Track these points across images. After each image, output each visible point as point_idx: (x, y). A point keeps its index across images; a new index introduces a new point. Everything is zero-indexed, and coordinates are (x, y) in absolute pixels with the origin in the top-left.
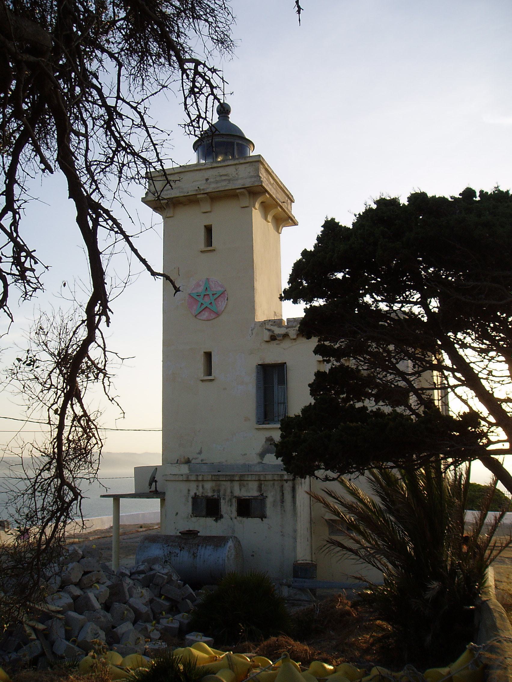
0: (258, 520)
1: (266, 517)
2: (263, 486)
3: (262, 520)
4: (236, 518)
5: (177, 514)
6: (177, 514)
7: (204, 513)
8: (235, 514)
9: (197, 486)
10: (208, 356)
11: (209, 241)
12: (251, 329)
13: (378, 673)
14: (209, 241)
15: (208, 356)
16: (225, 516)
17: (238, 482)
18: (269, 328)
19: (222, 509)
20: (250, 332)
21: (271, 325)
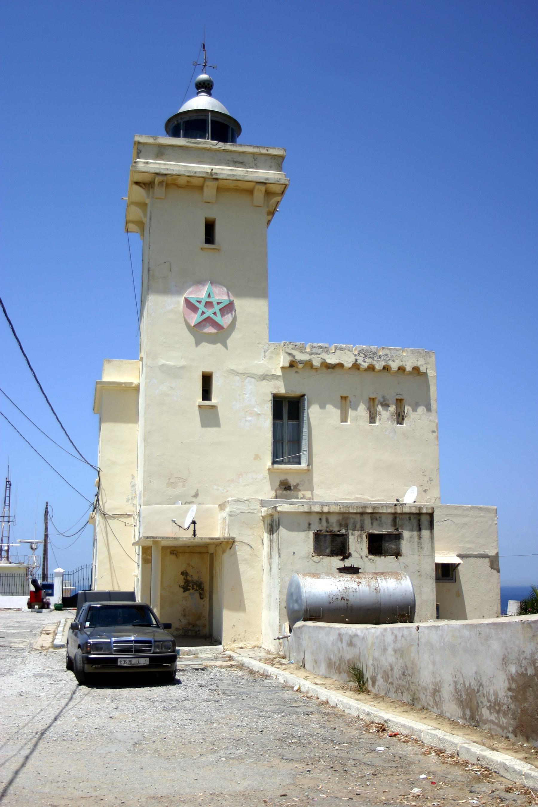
0: (392, 559)
1: (401, 556)
2: (398, 520)
3: (397, 558)
4: (367, 557)
5: (294, 553)
6: (294, 553)
7: (328, 551)
8: (366, 551)
9: (320, 519)
10: (207, 380)
11: (204, 48)
12: (263, 350)
13: (108, 520)
14: (204, 48)
15: (207, 380)
16: (354, 554)
17: (369, 515)
18: (290, 352)
19: (350, 547)
20: (263, 354)
21: (292, 349)
